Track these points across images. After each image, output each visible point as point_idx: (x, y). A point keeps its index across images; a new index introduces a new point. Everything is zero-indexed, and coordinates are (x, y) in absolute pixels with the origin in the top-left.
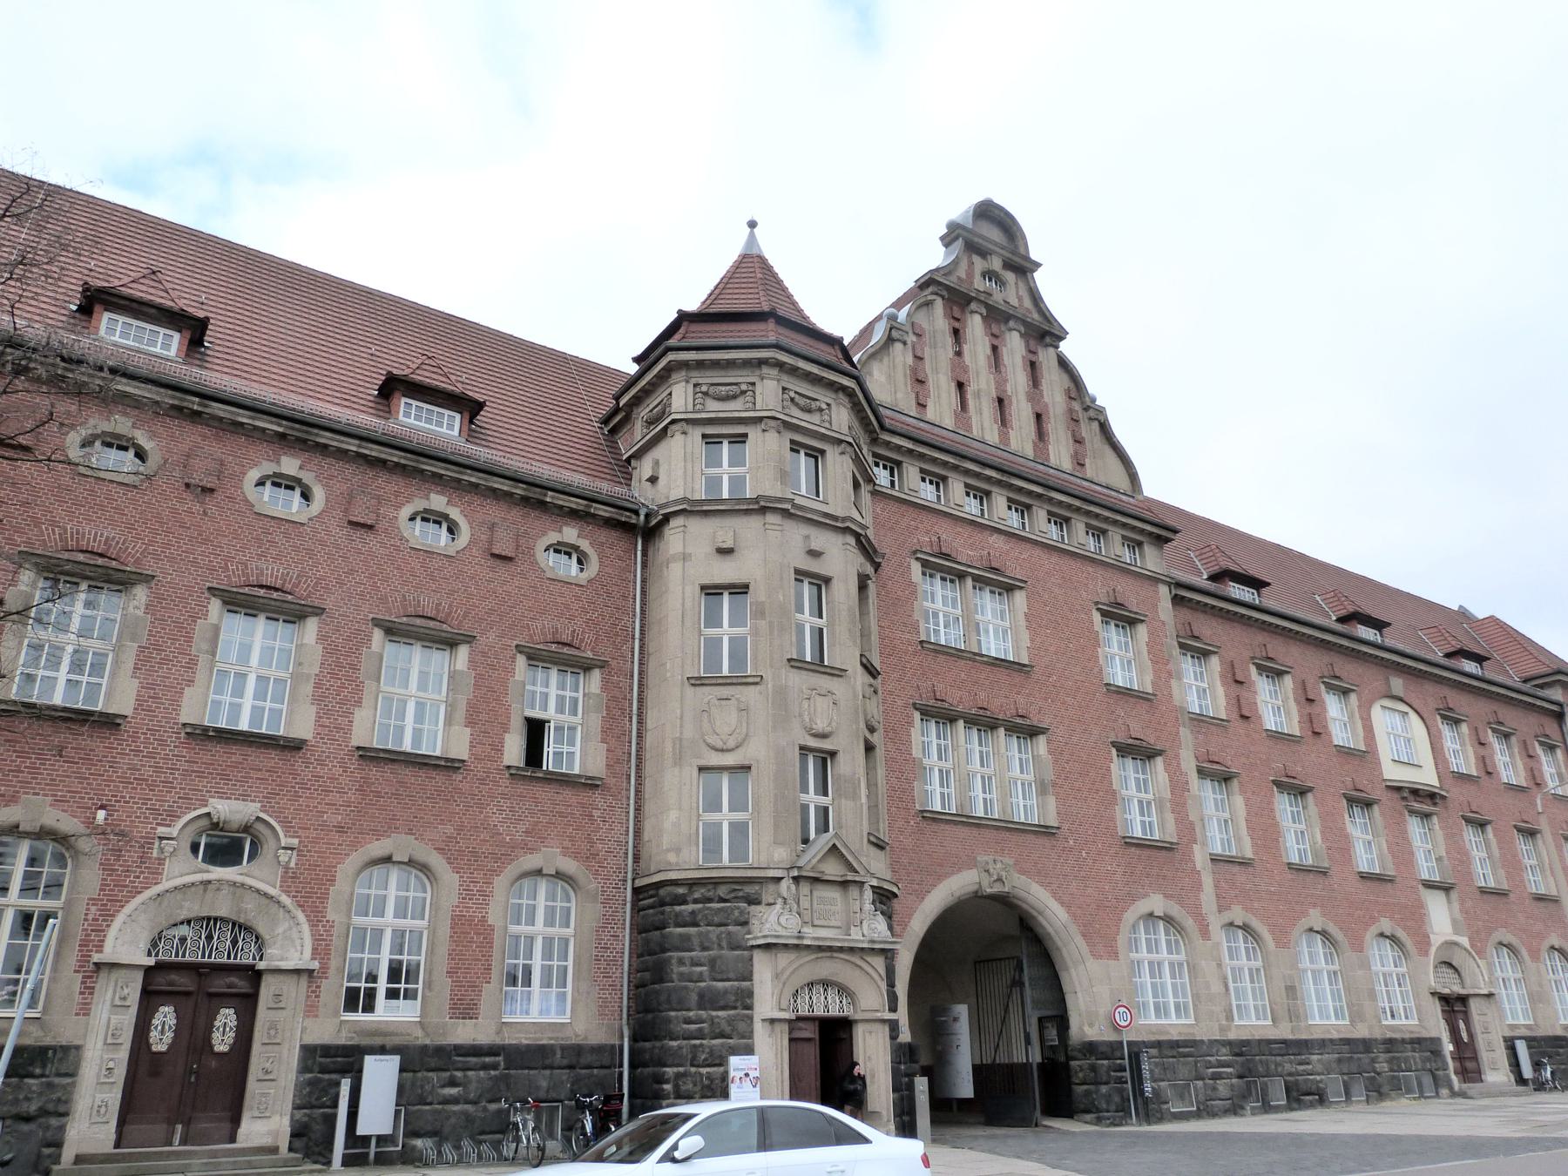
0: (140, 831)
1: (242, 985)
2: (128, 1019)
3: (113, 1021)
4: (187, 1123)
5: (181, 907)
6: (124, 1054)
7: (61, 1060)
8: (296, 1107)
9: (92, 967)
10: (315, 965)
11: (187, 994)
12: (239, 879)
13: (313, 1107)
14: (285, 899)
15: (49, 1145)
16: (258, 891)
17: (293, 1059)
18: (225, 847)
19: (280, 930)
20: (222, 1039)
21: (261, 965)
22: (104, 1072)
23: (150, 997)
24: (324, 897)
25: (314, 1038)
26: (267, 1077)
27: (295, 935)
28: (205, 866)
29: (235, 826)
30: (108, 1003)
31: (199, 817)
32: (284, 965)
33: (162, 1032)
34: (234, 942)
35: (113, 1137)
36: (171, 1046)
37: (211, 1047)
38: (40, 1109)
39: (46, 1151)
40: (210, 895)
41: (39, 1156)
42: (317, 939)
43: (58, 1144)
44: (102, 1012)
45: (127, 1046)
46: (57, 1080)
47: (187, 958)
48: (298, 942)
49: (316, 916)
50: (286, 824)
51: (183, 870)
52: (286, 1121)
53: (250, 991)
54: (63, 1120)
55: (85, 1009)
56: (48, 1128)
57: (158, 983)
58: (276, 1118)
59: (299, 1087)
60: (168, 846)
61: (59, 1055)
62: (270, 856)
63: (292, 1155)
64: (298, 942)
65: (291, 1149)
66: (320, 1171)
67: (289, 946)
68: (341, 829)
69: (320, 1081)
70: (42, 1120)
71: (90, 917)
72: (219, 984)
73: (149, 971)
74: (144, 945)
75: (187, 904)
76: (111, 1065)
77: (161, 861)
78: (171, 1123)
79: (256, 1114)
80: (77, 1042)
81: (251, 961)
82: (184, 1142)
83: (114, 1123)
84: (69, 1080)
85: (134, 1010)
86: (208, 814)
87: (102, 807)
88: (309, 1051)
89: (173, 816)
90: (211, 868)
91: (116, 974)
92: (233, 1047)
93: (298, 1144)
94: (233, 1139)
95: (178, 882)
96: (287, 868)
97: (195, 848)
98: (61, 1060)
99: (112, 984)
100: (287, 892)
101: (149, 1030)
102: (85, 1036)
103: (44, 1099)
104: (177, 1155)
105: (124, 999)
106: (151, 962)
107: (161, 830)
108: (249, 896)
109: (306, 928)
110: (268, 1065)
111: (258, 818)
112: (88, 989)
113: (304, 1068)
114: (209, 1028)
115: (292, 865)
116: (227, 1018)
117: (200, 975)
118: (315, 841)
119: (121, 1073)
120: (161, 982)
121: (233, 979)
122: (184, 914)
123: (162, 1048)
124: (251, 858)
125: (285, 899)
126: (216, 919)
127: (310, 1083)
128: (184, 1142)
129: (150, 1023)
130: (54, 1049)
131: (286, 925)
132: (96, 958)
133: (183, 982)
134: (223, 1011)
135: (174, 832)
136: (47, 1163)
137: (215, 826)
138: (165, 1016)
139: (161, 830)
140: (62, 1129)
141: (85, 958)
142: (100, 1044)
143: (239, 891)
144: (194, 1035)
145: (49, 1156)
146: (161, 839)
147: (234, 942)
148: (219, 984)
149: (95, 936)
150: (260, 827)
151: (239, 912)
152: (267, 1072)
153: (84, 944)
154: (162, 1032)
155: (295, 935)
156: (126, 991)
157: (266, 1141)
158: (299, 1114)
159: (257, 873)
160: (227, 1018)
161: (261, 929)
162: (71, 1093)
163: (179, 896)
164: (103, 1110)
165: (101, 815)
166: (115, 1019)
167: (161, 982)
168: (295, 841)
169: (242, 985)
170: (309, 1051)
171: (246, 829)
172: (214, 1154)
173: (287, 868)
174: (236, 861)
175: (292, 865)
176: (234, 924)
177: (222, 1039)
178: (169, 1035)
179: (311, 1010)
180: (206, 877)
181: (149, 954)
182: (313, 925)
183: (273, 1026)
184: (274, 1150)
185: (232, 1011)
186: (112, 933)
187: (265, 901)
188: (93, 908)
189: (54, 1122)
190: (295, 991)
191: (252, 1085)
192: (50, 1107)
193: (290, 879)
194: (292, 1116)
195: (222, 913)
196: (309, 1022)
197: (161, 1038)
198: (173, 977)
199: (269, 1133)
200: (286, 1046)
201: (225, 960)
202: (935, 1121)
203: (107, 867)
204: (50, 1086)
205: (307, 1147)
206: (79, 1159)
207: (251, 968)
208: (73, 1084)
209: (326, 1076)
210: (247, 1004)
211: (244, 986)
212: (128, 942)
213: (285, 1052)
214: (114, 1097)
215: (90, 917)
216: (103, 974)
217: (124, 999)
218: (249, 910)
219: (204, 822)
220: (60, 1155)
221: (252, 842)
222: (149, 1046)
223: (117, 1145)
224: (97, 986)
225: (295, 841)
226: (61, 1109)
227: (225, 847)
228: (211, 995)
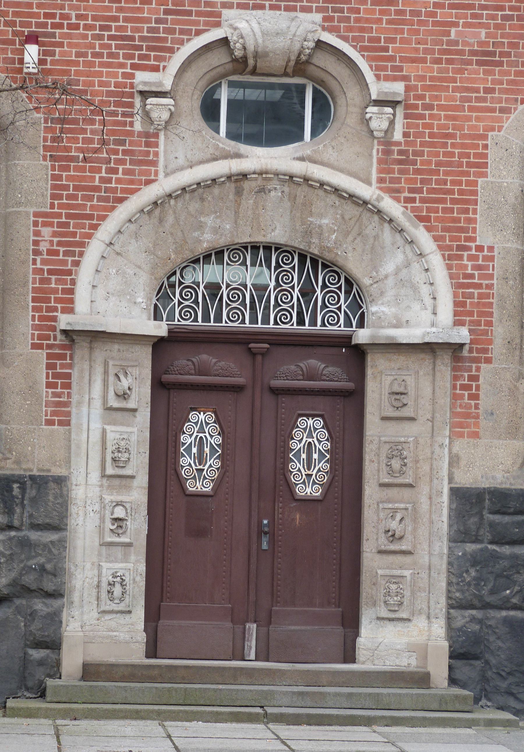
0: (103, 81)
1: (331, 373)
2: (136, 433)
3: (110, 436)
4: (266, 621)
5: (201, 226)
6: (138, 495)
7: (34, 501)
8: (455, 605)
9: (60, 339)
10: (462, 335)
11: (237, 389)
12: (298, 168)
13: (486, 606)
14: (392, 207)
15: (39, 645)
16: (336, 190)
17: (438, 515)
18: (272, 102)
19: (389, 267)
20: (309, 477)
21: (362, 336)
22: (109, 525)
23: (170, 396)
24: (468, 200)
25: (469, 478)
26: (395, 546)
27: (419, 277)
28: (232, 145)
29: (279, 63)
30: (97, 403)
31: (207, 48)
32: (403, 335)
33: (201, 458)
34: (307, 293)
35: (142, 637)
36: (218, 484)
37: (290, 488)
38: (14, 583)
39: (36, 654)
40: (248, 202)
41: (25, 660)
42: (461, 284)
43: (54, 645)
44: (89, 419)
45: (142, 479)
46: (34, 536)
47: (225, 323)
48: (425, 290)
49: (456, 242)
50: (374, 50)
51: (191, 155)
52: (439, 629)
53: (350, 385)
54: (56, 603)
55: (61, 415)
56: (33, 614)
57: (184, 367)
58: (421, 622)
59: (456, 569)
60: (160, 109)
61: (31, 493)
62: (352, 120)
63: (457, 691)
64: (425, 290)
65: (453, 681)
66: (506, 724)
67: (411, 300)
68: (487, 58)
69: (495, 557)
70: (18, 602)
71: (44, 247)
72: (289, 370)
73: (159, 345)
74: (144, 297)
75: (209, 221)
76: (120, 512)
77: (150, 138)
78: (239, 620)
79: (384, 613)
80: (57, 471)
81: (340, 328)
82: (263, 654)
83: (139, 613)
84: (54, 536)
85: (144, 416)
86: (225, 41)
87: (32, 39)
88: (467, 501)
89: (158, 50)
90: (244, 148)
91: (101, 353)
92: (328, 488)
93: (465, 671)
94: (349, 656)
95: (187, 177)
96: (387, 143)
97: (210, 111)
98: (34, 501)
99: (99, 370)
100: (394, 193)
101: (177, 455)
102: (68, 462)
103: (17, 567)
104: (250, 674)
105: (124, 396)
106: (160, 329)
107: (143, 78)
108: (321, 202)
109: (436, 261)
110: (394, 525)
111: (320, 44)
112: (61, 379)
113: (460, 535)
114: (282, 454)
115: (398, 136)
116: (310, 435)
117: (253, 354)
118: (437, 85)
119: (138, 527)
120: (185, 365)
121: (315, 363)
122: (207, 240)
123: (206, 487)
124: (314, 133)
125: (392, 207)
126: (268, 248)
127: (475, 561)
128: (263, 654)
129: (177, 444)
130: (20, 480)
131: (400, 258)
132: (64, 321)
133: (225, 366)
134: (193, 416)
135: (166, 79)
136: (39, 673)
137: (241, 64)
138: (201, 429)
139: (143, 78)
140: (55, 619)
141: (46, 324)
142: (95, 476)
143: (302, 192)
144: (256, 462)
145: (41, 663)
146: (145, 94)
147: (307, 293)
148: (289, 370)
149: (56, 288)
150: (323, 60)
151: (308, 233)
152: (393, 537)
153: (41, 297)
154: (201, 458)
155: (419, 277)
156: (125, 383)
157: (407, 662)
158: (462, 618)
159: (330, 155)
160: (310, 435)
161: (354, 264)
162: (61, 558)
163: (194, 206)
164: (117, 590)
165: (32, 52)
166: (114, 433)
167: (185, 365)
168: (398, 88)
169: (331, 373)
170: (467, 501)
171: (300, 66)
172: (313, 680)
173: (387, 143)
174: (294, 135)
175: (398, 136)
176: (302, 258)
177: (309, 477)
178: (213, 464)
179: (464, 422)
180: (235, 166)
181: (157, 316)
182: (452, 255)
183: (396, 451)
184: (422, 679)
185: (319, 423)
186: (85, 275)
187: (351, 210)
188: (46, 232)
189: (40, 606)
190: (429, 387)
191: (373, 563)
192: (29, 580)
193: (396, 164)
194: (449, 619)
195: (278, 235)
196: (459, 446)
197: (200, 471)
198: (206, 357)
199: (411, 648)
200: (424, 489)
201: (293, 326)
202: (68, 407)
203: (57, 155)
204: (25, 544)
205: (484, 679)
206: (90, 671)
207: (345, 341)
208: (62, 544)
209: (507, 550)
210: (346, 407)
211: (336, 373)
212: (114, 293)
213: (424, 501)
214: (134, 568)
215: (44, 247)
216: (81, 351)
217: (124, 396)
218: (328, 230)
219: (218, 59)
220: (58, 664)
221: (318, 97)
222: (181, 482)
223: (152, 651)
224: (75, 374)
225: (398, 88)
226: (49, 586)
227: (272, 102)
228: (276, 392)
